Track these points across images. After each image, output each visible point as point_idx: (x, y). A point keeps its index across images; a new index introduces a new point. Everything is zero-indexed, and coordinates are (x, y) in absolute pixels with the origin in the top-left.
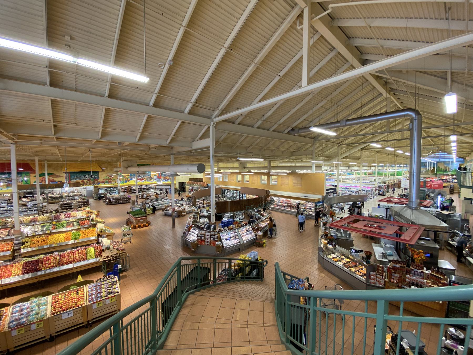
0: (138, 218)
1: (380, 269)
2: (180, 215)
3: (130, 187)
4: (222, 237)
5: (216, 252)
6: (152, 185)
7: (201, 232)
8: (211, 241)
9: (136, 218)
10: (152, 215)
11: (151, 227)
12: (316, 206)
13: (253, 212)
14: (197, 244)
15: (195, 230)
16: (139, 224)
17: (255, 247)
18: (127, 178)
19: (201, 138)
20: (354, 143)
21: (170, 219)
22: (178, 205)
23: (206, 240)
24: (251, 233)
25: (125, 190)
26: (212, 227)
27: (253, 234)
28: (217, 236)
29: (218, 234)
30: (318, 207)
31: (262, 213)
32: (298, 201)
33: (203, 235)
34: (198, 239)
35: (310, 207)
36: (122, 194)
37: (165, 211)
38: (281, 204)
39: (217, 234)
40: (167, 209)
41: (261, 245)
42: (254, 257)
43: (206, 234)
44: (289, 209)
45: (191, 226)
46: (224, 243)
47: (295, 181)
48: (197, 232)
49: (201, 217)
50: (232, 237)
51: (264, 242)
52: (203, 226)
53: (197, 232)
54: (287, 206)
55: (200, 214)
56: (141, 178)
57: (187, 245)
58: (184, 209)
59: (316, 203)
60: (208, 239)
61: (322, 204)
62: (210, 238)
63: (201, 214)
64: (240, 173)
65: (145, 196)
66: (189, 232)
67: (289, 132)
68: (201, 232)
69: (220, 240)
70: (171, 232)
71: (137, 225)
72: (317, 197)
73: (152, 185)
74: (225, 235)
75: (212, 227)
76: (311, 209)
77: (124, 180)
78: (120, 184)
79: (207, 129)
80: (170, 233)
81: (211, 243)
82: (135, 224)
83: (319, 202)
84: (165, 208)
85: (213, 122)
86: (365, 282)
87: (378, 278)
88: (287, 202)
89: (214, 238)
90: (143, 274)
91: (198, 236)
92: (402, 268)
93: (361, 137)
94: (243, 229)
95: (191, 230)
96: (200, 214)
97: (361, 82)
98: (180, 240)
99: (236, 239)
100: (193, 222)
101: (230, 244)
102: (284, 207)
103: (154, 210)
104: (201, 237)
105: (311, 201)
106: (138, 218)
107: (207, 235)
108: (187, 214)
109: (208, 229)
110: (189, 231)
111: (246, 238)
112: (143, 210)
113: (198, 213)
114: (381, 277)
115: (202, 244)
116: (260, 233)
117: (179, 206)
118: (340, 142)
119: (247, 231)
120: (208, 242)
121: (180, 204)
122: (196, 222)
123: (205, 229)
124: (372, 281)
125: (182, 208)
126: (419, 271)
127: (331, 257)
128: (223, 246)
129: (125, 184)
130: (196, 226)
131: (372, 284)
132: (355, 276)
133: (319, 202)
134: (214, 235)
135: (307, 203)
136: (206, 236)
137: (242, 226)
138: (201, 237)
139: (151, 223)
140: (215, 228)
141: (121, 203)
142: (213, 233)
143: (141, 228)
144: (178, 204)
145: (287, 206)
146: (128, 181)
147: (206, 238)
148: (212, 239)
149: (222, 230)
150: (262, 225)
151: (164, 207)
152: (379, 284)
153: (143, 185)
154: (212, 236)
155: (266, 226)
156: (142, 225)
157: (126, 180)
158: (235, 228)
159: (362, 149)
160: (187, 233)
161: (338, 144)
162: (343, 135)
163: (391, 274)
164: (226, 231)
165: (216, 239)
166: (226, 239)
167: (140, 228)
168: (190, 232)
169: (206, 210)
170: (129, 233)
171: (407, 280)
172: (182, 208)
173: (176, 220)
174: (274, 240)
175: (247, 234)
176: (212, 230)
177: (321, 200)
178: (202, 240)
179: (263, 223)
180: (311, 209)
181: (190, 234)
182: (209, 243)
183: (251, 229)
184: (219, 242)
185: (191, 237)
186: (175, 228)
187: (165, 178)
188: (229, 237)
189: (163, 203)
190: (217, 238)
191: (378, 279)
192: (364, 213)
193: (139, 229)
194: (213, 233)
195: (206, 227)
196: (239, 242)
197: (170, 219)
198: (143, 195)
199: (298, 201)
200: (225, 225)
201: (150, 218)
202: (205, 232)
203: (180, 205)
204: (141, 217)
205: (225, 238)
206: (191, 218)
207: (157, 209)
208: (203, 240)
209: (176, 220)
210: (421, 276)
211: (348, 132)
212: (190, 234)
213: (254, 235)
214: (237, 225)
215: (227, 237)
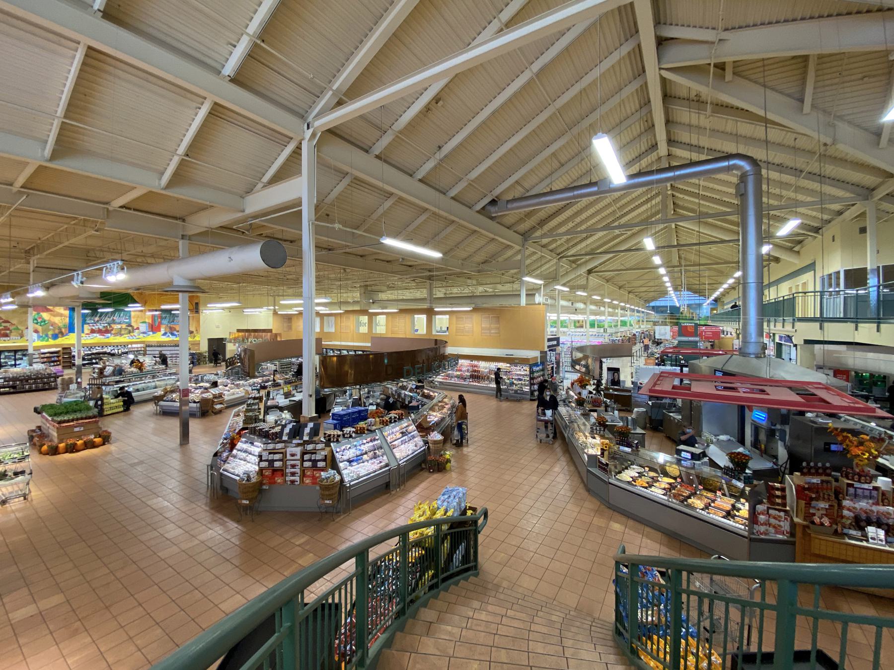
0: (68, 421)
1: (778, 493)
2: (207, 410)
3: (67, 350)
4: (338, 456)
5: (321, 502)
6: (134, 346)
7: (271, 446)
8: (303, 471)
9: (60, 423)
10: (123, 414)
11: (111, 448)
12: (532, 372)
13: (403, 392)
14: (261, 483)
15: (252, 443)
16: (70, 442)
17: (426, 474)
18: (60, 329)
19: (277, 178)
20: (586, 254)
21: (174, 424)
22: (201, 384)
23: (289, 470)
24: (413, 437)
25: (51, 358)
26: (307, 430)
27: (419, 441)
28: (323, 453)
29: (328, 449)
30: (536, 375)
31: (426, 391)
32: (493, 366)
33: (277, 457)
34: (261, 470)
35: (518, 375)
36: (38, 367)
37: (162, 403)
38: (458, 373)
39: (323, 449)
40: (169, 397)
41: (440, 467)
42: (459, 504)
43: (290, 450)
44: (474, 384)
45: (239, 433)
46: (344, 472)
47: (486, 325)
48: (258, 447)
49: (268, 410)
50: (366, 453)
51: (447, 457)
52: (278, 429)
53: (259, 450)
54: (472, 377)
55: (266, 403)
56: (101, 327)
57: (225, 490)
58: (220, 396)
59: (531, 367)
60: (293, 466)
61: (541, 367)
62: (303, 461)
63: (269, 403)
64: (364, 312)
65: (109, 370)
66: (231, 450)
67: (483, 208)
68: (271, 446)
69: (333, 464)
70: (177, 455)
71: (62, 445)
72: (533, 354)
73: (134, 346)
74: (345, 451)
75: (307, 430)
76: (520, 380)
77: (50, 333)
78: (34, 342)
79: (294, 152)
80: (175, 461)
81: (303, 475)
82: (56, 440)
83: (536, 365)
84: (164, 396)
85: (311, 130)
86: (746, 534)
87: (775, 518)
88: (471, 369)
89: (315, 462)
90: (42, 617)
91: (261, 460)
92: (825, 485)
93: (617, 232)
94: (394, 430)
95: (240, 445)
96: (266, 403)
97: (631, 110)
98: (202, 476)
99: (375, 457)
100: (245, 422)
101: (363, 472)
102: (465, 379)
103: (128, 401)
104: (273, 461)
105: (523, 361)
106: (68, 421)
107: (293, 455)
108: (227, 408)
109: (294, 437)
110: (233, 446)
111: (401, 451)
112: (92, 403)
113: (260, 399)
114: (782, 514)
115: (275, 483)
116: (436, 436)
117: (206, 389)
118: (562, 252)
119: (403, 434)
120: (293, 474)
121: (207, 382)
122: (257, 420)
123: (285, 438)
124: (763, 529)
125: (215, 391)
126: (866, 486)
127: (627, 475)
128: (342, 480)
129: (51, 342)
130: (254, 431)
131: (763, 537)
132: (711, 520)
133: (536, 365)
134: (313, 452)
135: (513, 367)
136: (289, 457)
137: (391, 422)
138: (271, 462)
139: (114, 435)
140: (315, 432)
141: (30, 391)
142: (310, 447)
143: (78, 451)
144: (202, 381)
145: (472, 377)
146: (63, 335)
147: (289, 463)
148: (307, 464)
149: (339, 436)
150: (434, 417)
151: (159, 392)
152: (777, 533)
153: (110, 345)
154: (306, 457)
155: (443, 419)
156: (80, 442)
157: (57, 331)
158: (374, 428)
159: (590, 272)
160: (225, 454)
161: (558, 255)
162: (584, 227)
163: (808, 505)
164: (351, 436)
165: (321, 464)
166: (350, 461)
167: (72, 452)
168: (235, 452)
169: (281, 392)
170: (19, 467)
171: (846, 513)
172: (215, 391)
173: (195, 425)
174: (465, 450)
175: (403, 442)
176: (306, 438)
177: (539, 361)
178: (275, 471)
179: (435, 414)
180: (520, 380)
181: (235, 457)
182: (297, 478)
183: (413, 427)
184: (332, 472)
185: (237, 465)
186: (191, 445)
187: (171, 328)
188: (358, 453)
189: (158, 383)
190: (325, 460)
191: (772, 521)
192: (624, 382)
193: (68, 456)
194: (310, 447)
195: (287, 430)
196: (387, 465)
197: (174, 424)
198: (104, 368)
199: (493, 366)
200: (342, 422)
201: (113, 426)
202: (286, 447)
203: (208, 385)
204: (77, 419)
205: (345, 458)
206: (238, 415)
207: (136, 399)
208: (281, 472)
209: (195, 425)
210: (871, 497)
211: (594, 220)
212: (235, 457)
213: (421, 443)
214: (378, 419)
215: (351, 454)
